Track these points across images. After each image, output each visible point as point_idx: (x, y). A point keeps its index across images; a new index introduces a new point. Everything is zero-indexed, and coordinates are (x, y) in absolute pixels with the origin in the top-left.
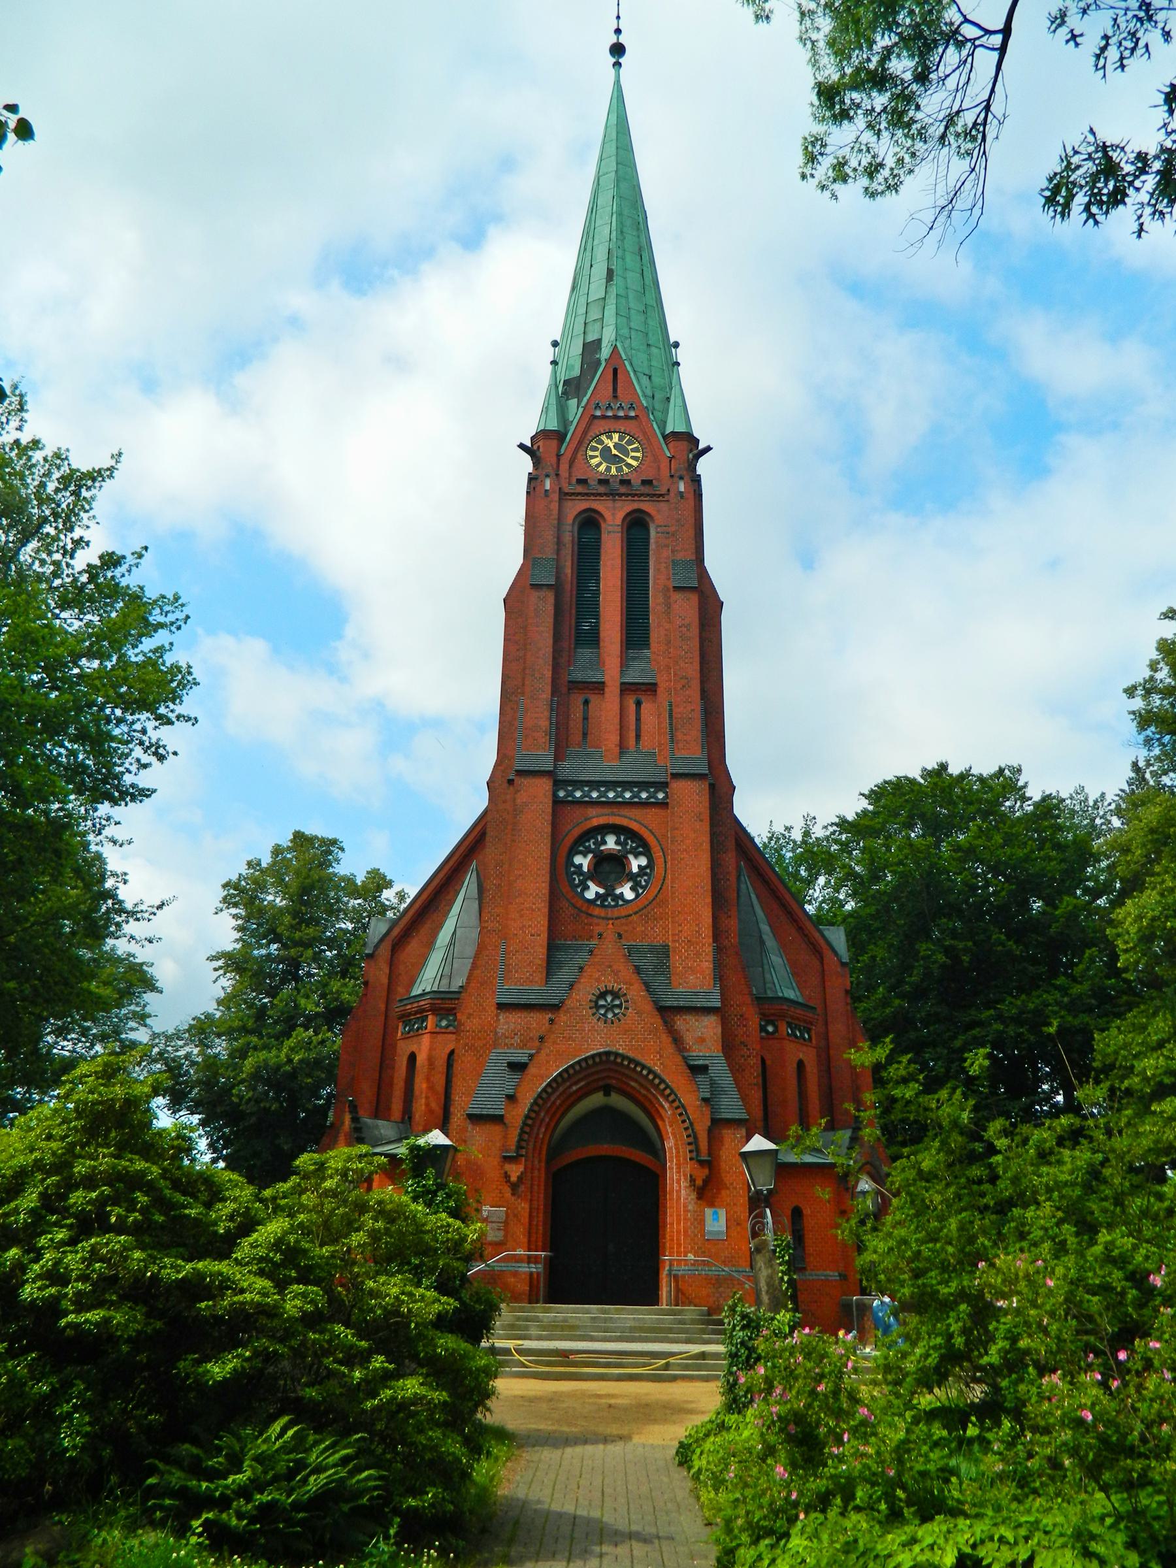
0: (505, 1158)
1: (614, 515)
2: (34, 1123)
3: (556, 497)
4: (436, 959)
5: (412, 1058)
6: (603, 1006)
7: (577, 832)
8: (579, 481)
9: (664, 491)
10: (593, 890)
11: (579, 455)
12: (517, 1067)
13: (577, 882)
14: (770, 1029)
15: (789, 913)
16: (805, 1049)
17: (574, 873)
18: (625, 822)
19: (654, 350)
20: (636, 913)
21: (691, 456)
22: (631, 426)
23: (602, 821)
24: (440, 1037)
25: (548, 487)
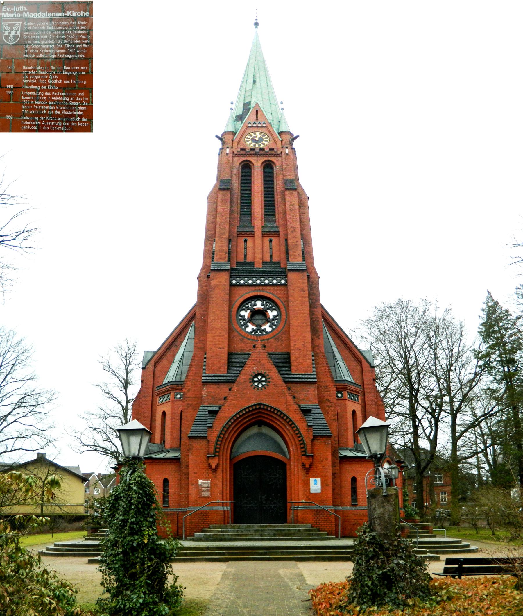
0: (208, 457)
1: (257, 163)
4: (174, 367)
5: (164, 413)
6: (256, 381)
7: (241, 300)
8: (242, 149)
9: (279, 152)
10: (250, 328)
11: (242, 140)
12: (214, 413)
13: (242, 324)
14: (339, 395)
15: (345, 344)
16: (356, 404)
17: (241, 319)
18: (266, 294)
20: (272, 338)
22: (264, 130)
23: (254, 294)
24: (177, 403)
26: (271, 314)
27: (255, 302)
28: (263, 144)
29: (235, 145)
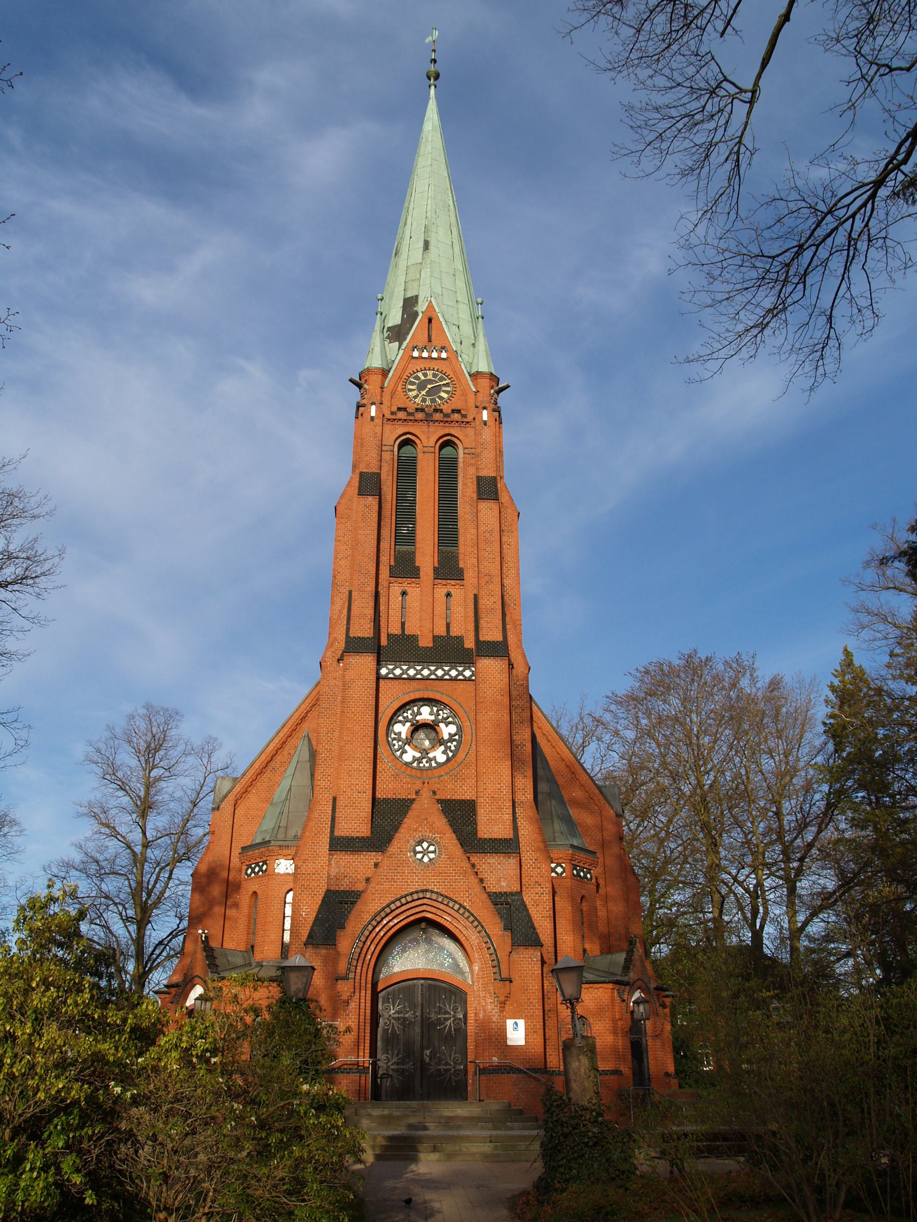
1: (428, 437)
2: (344, 988)
3: (378, 421)
10: (410, 755)
19: (461, 306)
21: (492, 391)
25: (373, 414)
26: (447, 731)
27: (419, 709)
28: (441, 398)
29: (386, 398)
